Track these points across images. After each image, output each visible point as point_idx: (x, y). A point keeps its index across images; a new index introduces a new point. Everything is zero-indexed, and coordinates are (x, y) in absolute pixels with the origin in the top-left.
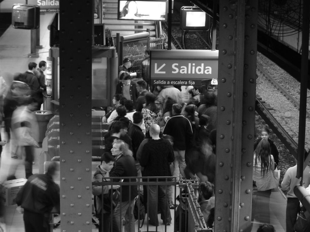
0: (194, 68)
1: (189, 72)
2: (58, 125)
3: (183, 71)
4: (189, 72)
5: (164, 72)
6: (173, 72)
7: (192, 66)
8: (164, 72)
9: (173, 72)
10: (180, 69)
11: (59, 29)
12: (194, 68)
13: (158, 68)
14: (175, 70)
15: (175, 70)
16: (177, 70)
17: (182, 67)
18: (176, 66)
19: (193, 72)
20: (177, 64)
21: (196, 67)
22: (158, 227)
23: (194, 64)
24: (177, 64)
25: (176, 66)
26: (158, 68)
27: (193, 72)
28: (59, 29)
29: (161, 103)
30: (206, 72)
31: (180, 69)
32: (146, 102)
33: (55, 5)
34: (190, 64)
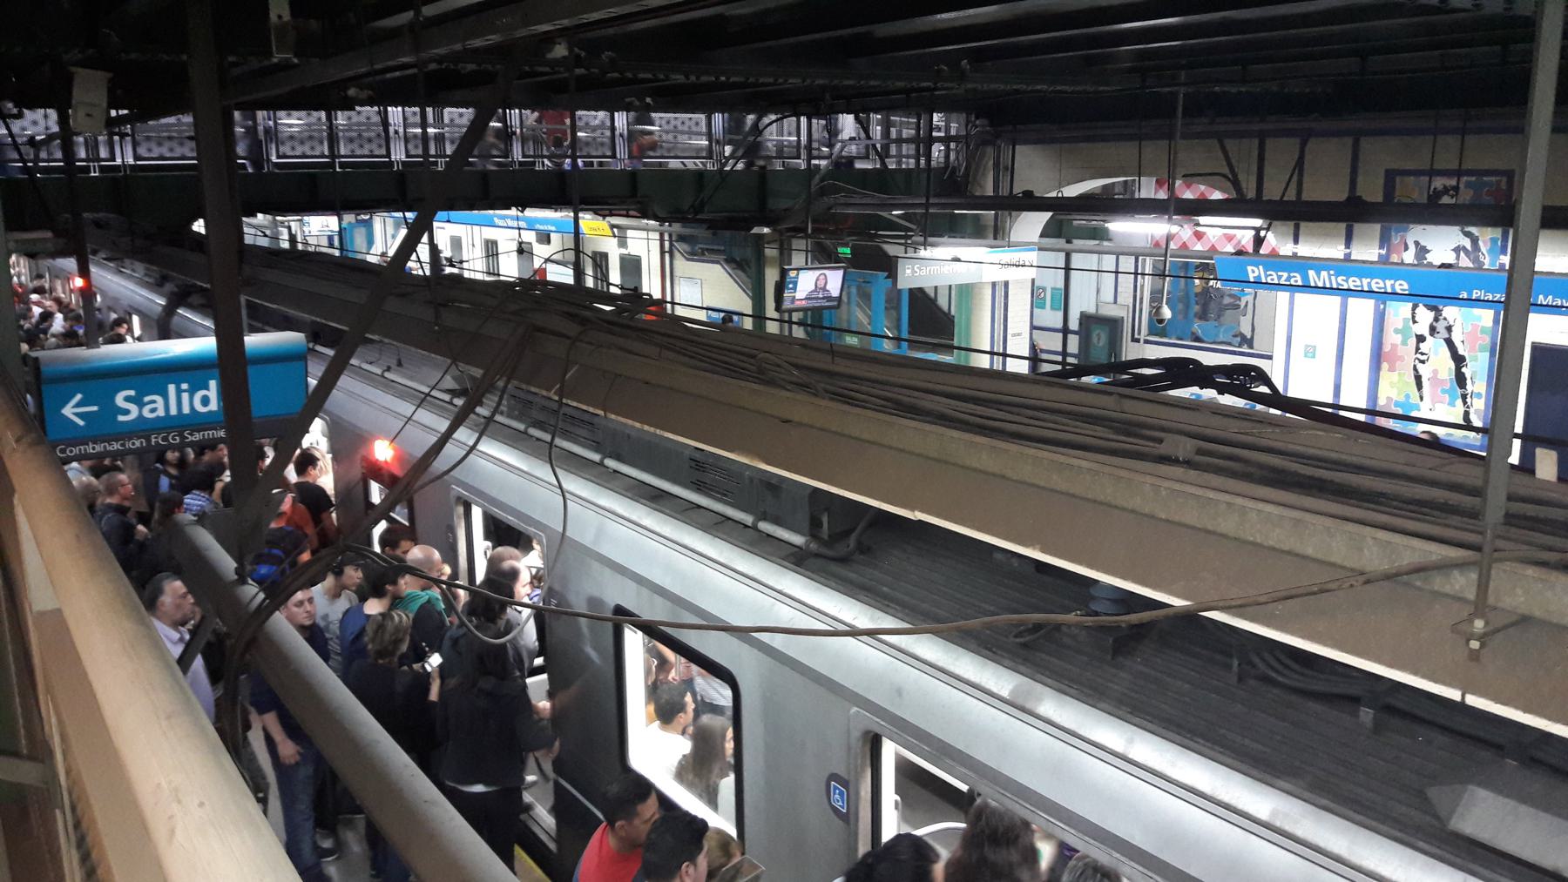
0: (185, 396)
1: (173, 411)
2: (730, 119)
3: (153, 410)
4: (173, 411)
5: (81, 423)
6: (121, 418)
7: (179, 392)
8: (81, 423)
9: (121, 418)
10: (141, 405)
11: (95, 408)
12: (185, 396)
13: (78, 405)
14: (127, 412)
15: (127, 412)
16: (133, 408)
17: (147, 399)
18: (127, 399)
19: (186, 410)
20: (132, 393)
21: (192, 392)
22: (640, 633)
23: (185, 386)
24: (132, 393)
25: (127, 399)
26: (78, 405)
27: (186, 410)
28: (95, 408)
29: (444, 306)
30: (146, 413)
31: (141, 405)
32: (489, 132)
33: (140, 416)
34: (172, 388)
